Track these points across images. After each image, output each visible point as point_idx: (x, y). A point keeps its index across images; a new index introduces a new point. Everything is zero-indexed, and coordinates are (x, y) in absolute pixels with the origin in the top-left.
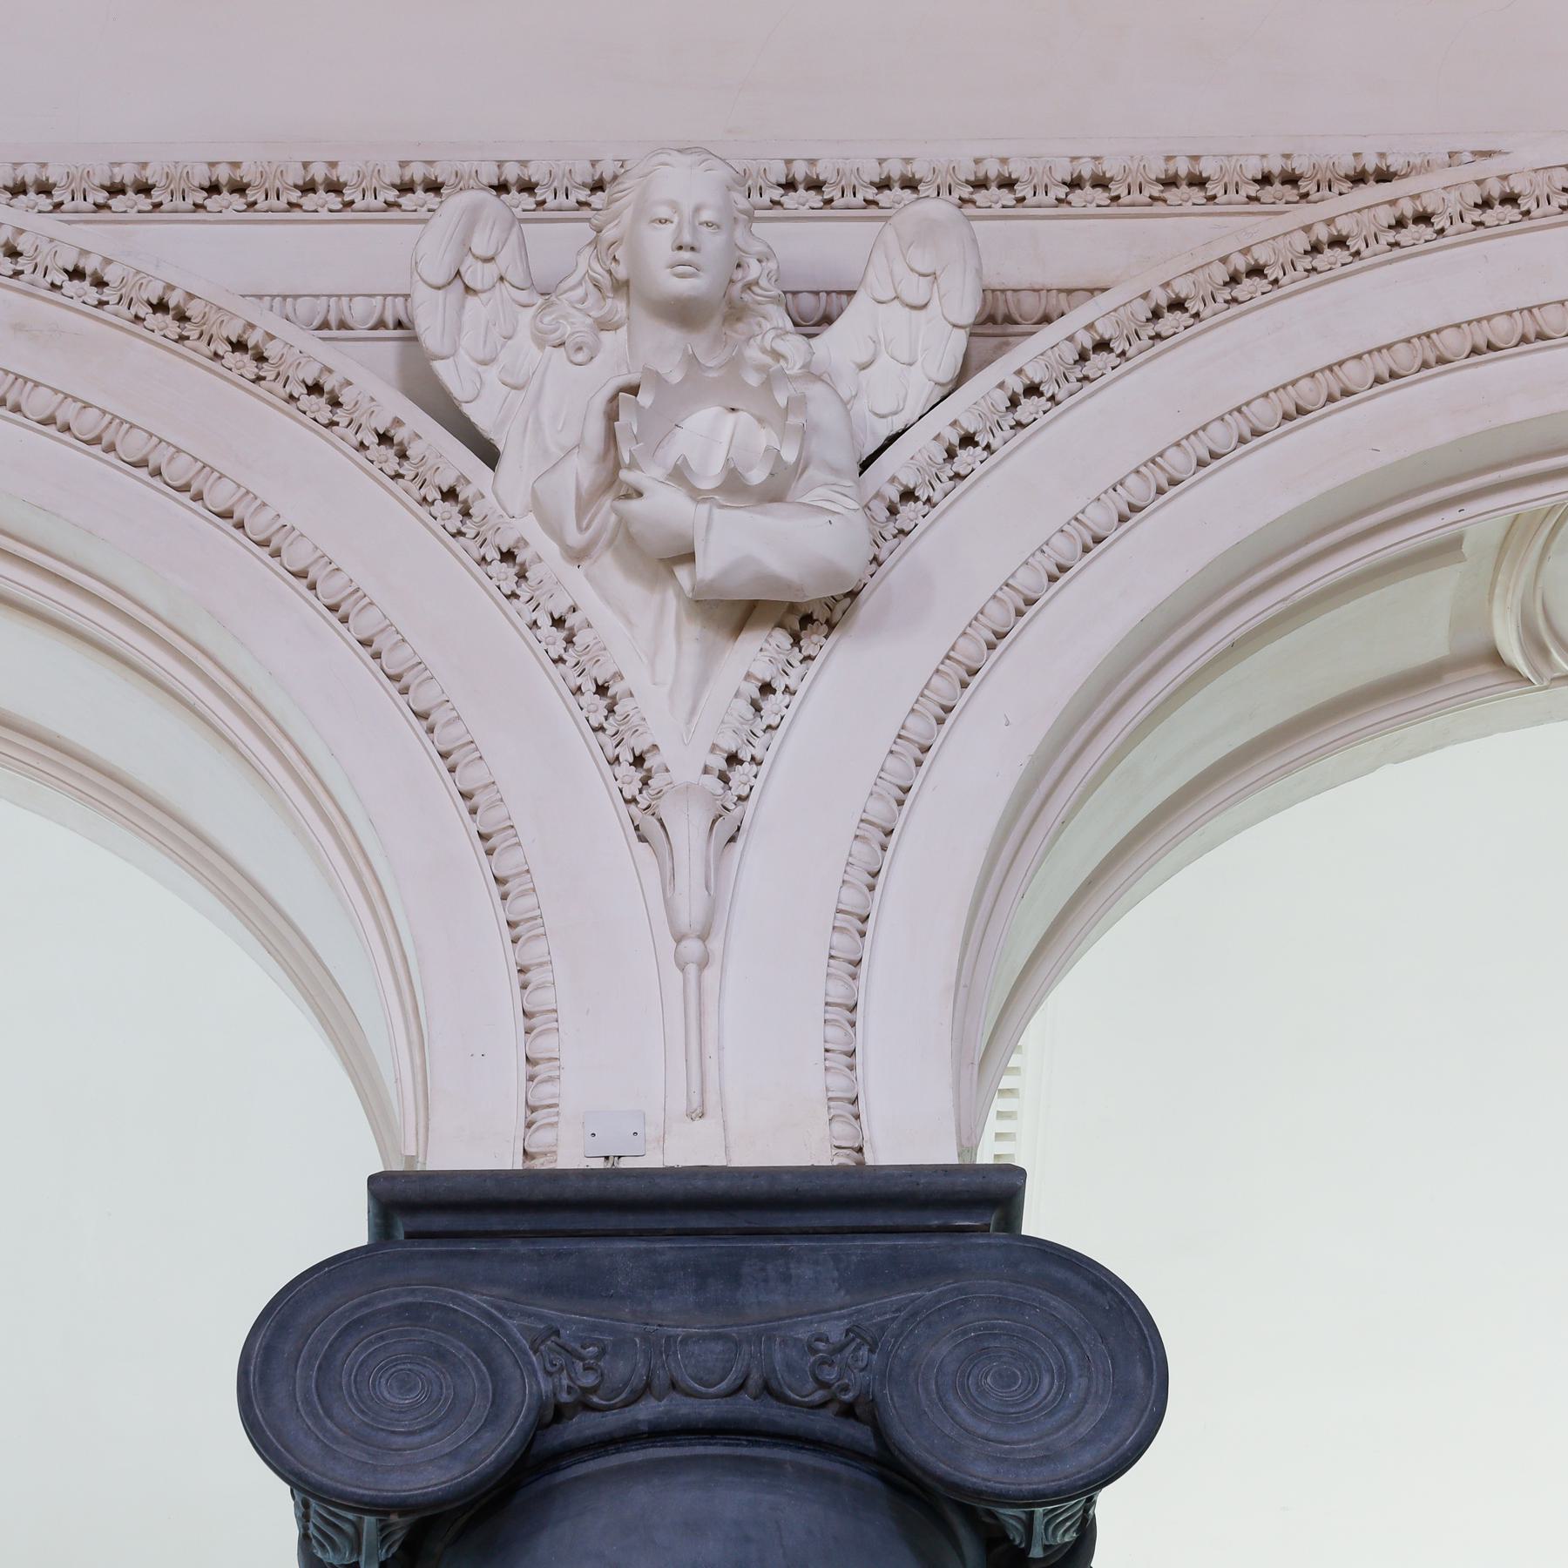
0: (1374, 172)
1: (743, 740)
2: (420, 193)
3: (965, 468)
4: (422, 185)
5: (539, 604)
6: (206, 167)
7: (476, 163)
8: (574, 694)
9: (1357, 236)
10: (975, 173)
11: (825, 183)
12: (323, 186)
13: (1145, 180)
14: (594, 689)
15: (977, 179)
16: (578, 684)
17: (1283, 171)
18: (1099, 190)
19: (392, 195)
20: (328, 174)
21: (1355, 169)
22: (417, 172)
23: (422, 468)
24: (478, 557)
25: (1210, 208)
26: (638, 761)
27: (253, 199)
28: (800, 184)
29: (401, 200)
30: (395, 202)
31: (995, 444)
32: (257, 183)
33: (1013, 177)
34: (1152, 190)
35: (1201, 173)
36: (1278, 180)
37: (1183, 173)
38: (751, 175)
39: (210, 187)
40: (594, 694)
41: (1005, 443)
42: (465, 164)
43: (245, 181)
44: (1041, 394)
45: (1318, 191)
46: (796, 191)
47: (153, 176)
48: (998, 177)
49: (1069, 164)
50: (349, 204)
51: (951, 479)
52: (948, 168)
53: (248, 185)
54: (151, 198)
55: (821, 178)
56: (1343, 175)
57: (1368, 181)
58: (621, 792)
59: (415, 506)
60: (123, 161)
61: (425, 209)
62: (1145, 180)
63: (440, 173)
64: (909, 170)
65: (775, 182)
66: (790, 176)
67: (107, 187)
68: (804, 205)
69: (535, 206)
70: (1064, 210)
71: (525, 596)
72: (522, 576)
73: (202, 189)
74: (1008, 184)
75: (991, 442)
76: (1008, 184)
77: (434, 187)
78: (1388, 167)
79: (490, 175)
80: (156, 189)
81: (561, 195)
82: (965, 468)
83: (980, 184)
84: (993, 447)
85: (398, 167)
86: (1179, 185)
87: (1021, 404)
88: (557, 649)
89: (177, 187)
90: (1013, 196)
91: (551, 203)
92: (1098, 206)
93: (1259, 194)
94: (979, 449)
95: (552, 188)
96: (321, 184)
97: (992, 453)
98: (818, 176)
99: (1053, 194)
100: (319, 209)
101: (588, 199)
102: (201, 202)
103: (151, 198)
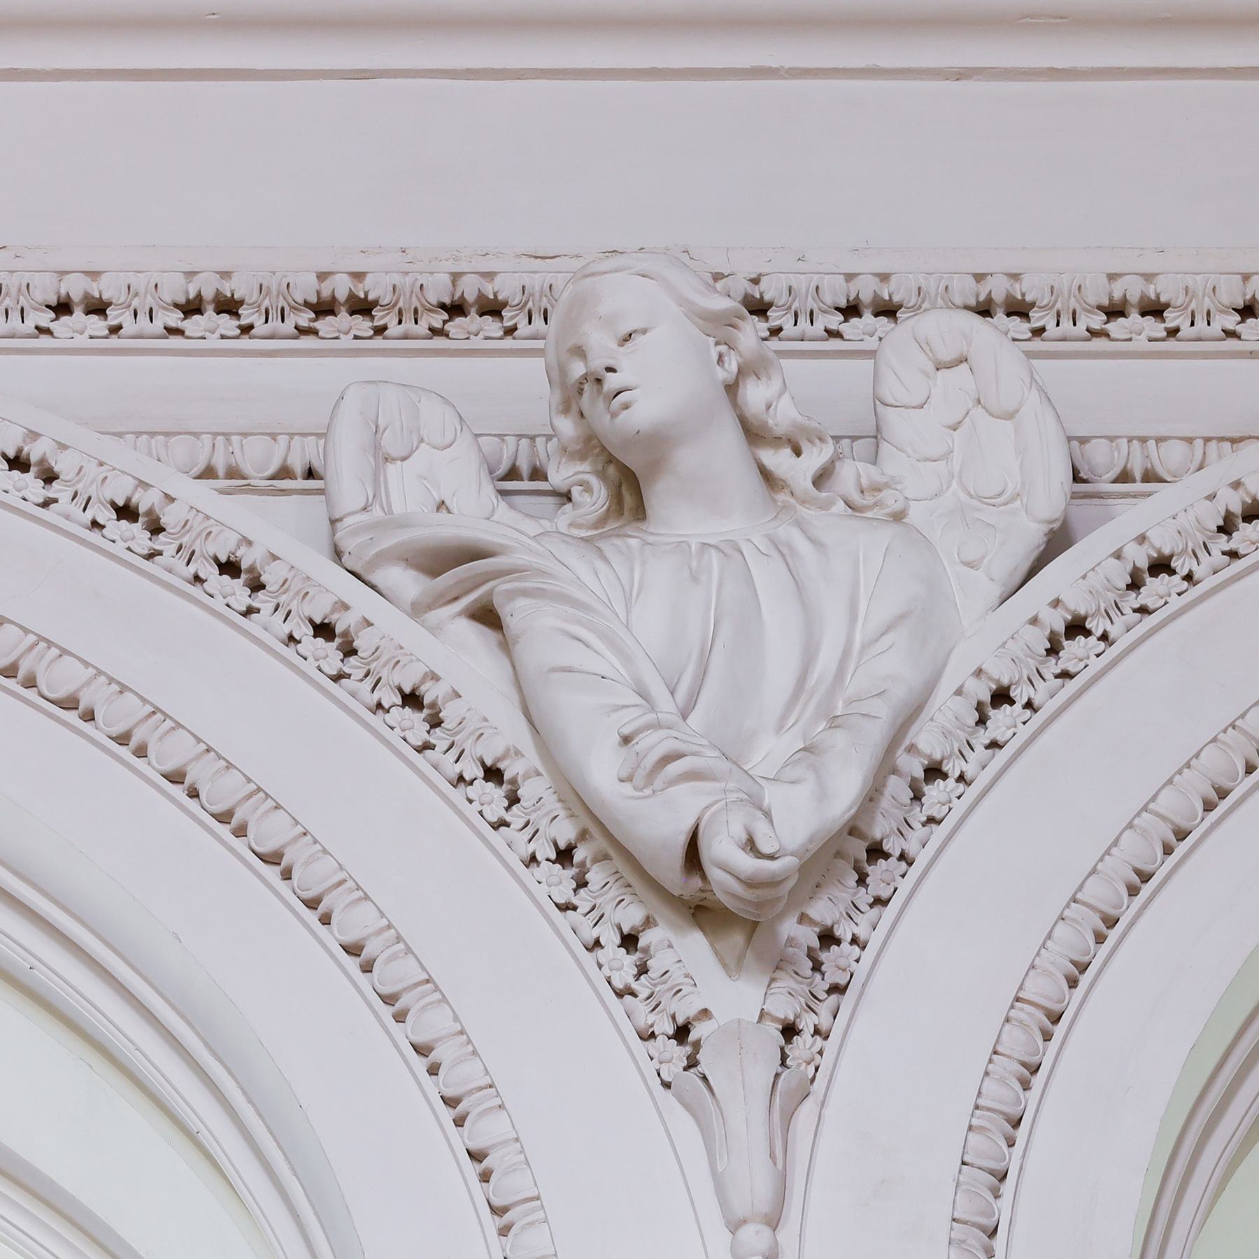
0: (347, 301)
1: (801, 1005)
2: (1135, 317)
3: (1076, 664)
4: (83, 306)
5: (537, 831)
6: (972, 280)
7: (1213, 276)
8: (527, 866)
9: (1184, 551)
10: (318, 293)
11: (1167, 306)
12: (346, 307)
13: (423, 305)
14: (618, 940)
15: (188, 301)
16: (530, 851)
17: (1143, 297)
18: (1016, 319)
19: (1098, 321)
20: (352, 288)
21: (977, 296)
22: (866, 290)
23: (375, 663)
24: (454, 776)
25: (245, 343)
26: (681, 1033)
27: (381, 323)
28: (471, 306)
29: (317, 325)
30: (1102, 329)
31: (1113, 632)
32: (515, 302)
33: (1163, 299)
34: (167, 318)
35: (1158, 296)
36: (870, 310)
37: (342, 295)
38: (269, 293)
39: (847, 307)
40: (619, 947)
41: (1128, 631)
42: (1198, 278)
43: (371, 297)
44: (1172, 572)
45: (400, 322)
46: (861, 317)
47: (239, 289)
48: (1142, 299)
49: (844, 284)
50: (380, 331)
51: (1057, 677)
52: (413, 285)
53: (375, 303)
54: (239, 320)
55: (105, 297)
56: (435, 303)
57: (206, 311)
58: (659, 1074)
59: (368, 716)
60: (1156, 271)
61: (1144, 336)
62: (423, 305)
63: (895, 291)
64: (96, 289)
65: (169, 301)
66: (458, 295)
67: (182, 305)
68: (476, 335)
69: (107, 332)
70: (439, 342)
71: (517, 823)
72: (513, 800)
73: (837, 309)
74: (1155, 310)
75: (1108, 629)
76: (1155, 310)
77: (888, 311)
78: (366, 294)
79: (967, 291)
80: (1170, 309)
81: (1201, 323)
82: (1076, 664)
83: (1115, 311)
84: (1111, 636)
85: (316, 280)
86: (993, 314)
87: (1145, 585)
88: (565, 892)
89: (407, 306)
90: (370, 324)
91: (260, 328)
92: (223, 337)
93: (181, 325)
94: (1093, 639)
95: (1055, 310)
96: (343, 305)
97: (1111, 645)
98: (495, 296)
99: (822, 322)
100: (207, 335)
101: (311, 324)
102: (1232, 328)
103: (1029, 321)
